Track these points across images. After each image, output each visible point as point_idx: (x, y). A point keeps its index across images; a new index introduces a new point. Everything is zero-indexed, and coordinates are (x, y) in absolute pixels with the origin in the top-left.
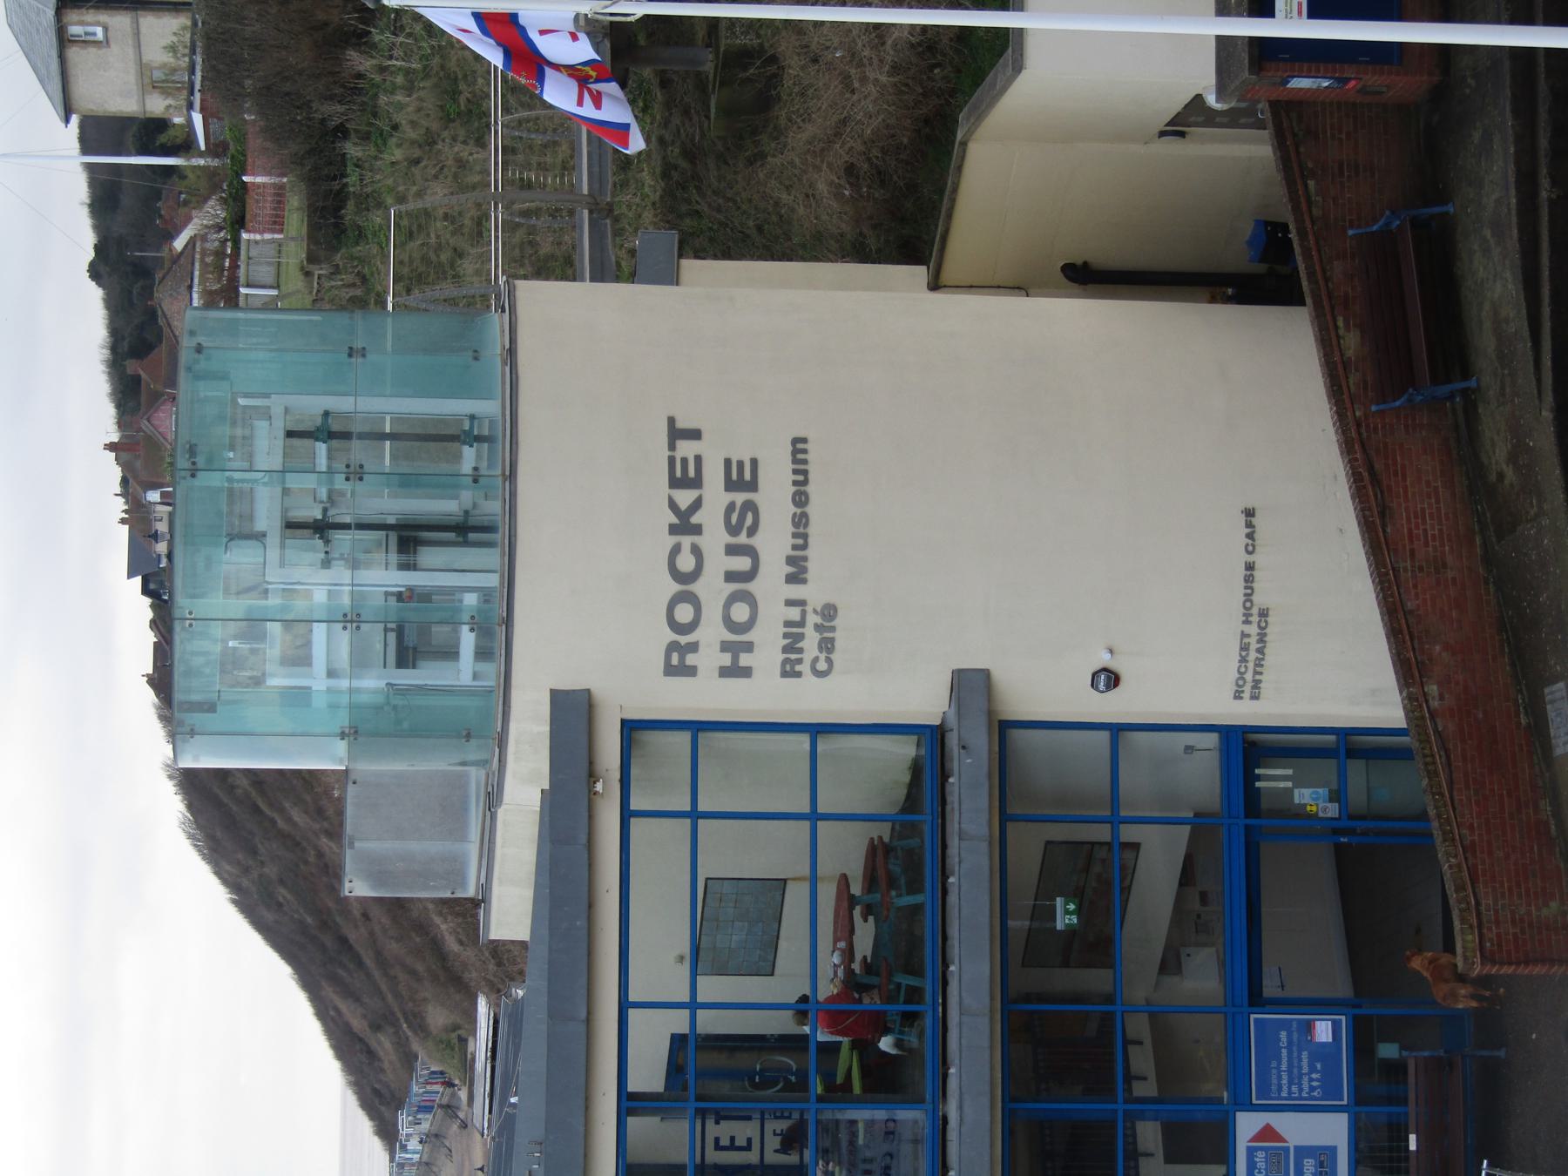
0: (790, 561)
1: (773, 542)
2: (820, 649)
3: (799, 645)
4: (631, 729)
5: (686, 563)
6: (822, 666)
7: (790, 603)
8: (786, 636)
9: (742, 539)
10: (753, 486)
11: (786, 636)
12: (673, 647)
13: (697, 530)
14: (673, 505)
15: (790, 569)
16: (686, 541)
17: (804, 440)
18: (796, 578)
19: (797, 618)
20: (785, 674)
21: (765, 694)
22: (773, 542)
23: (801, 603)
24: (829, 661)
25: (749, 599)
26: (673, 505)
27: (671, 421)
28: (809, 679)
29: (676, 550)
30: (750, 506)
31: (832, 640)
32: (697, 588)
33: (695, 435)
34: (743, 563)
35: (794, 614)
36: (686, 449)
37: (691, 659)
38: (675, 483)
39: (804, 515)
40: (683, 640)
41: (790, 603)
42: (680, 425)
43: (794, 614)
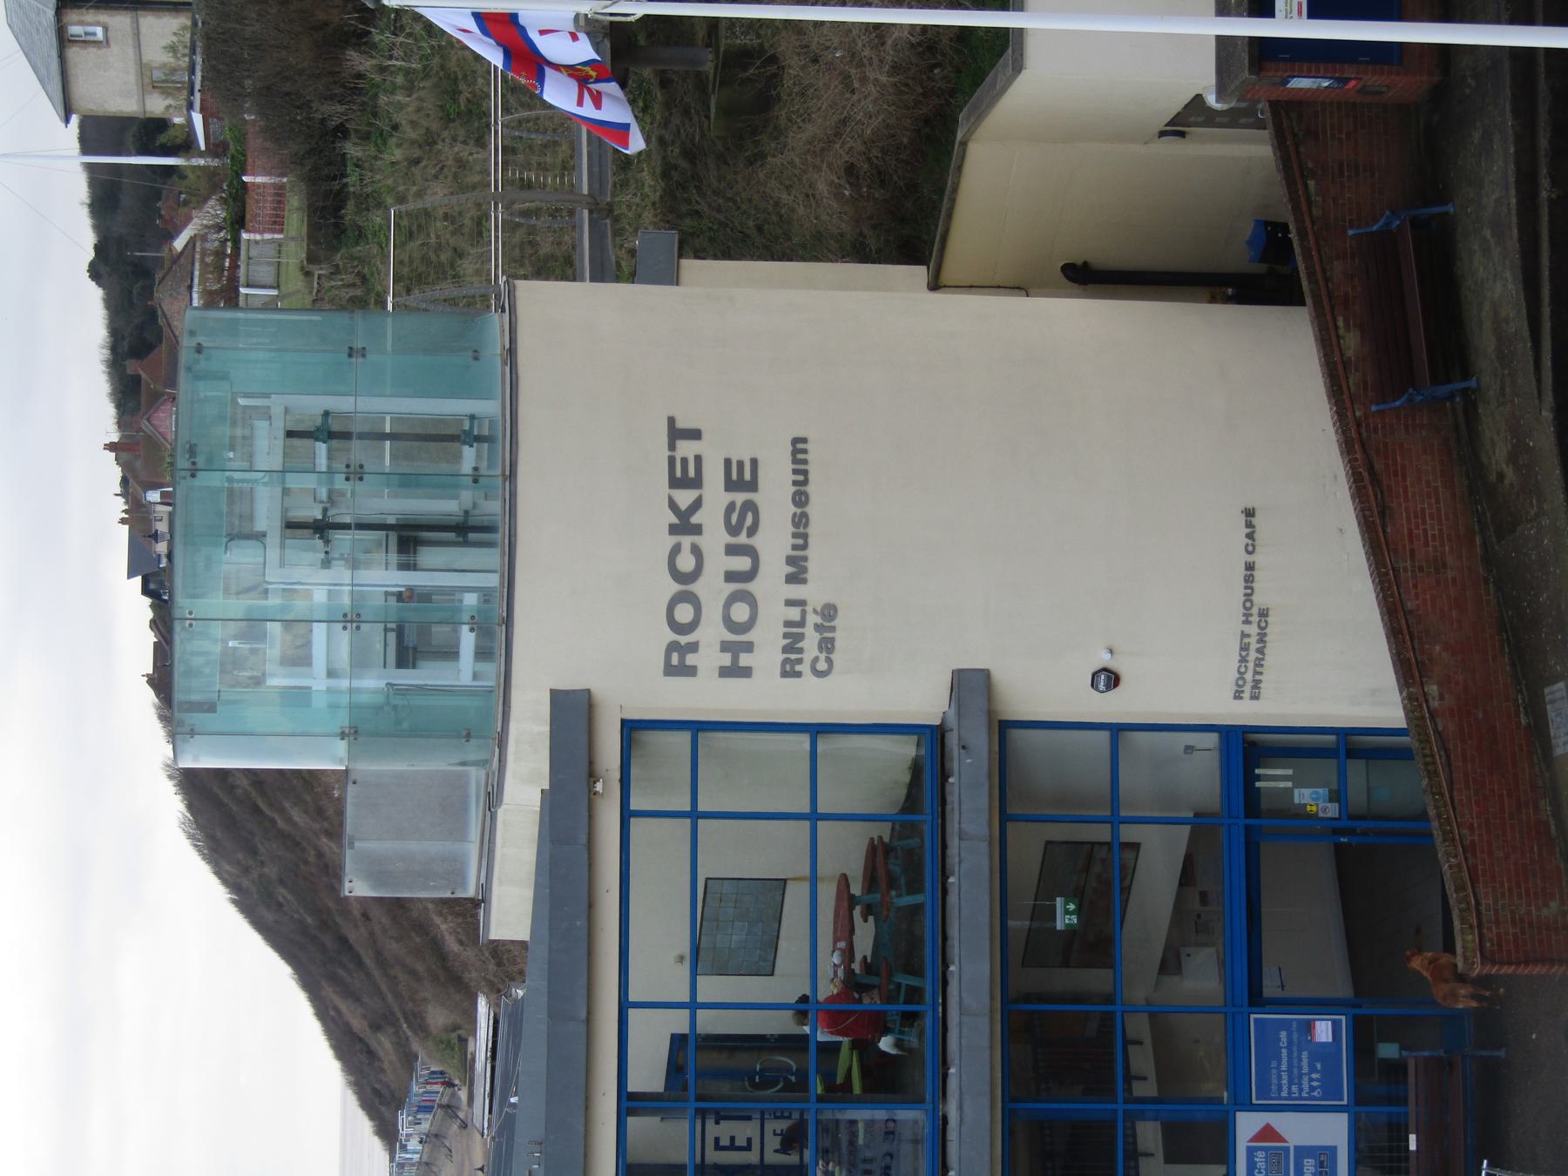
0: (790, 561)
1: (773, 542)
2: (820, 649)
3: (799, 645)
4: (631, 729)
5: (686, 563)
6: (822, 666)
7: (790, 603)
8: (786, 636)
9: (742, 539)
10: (753, 486)
11: (786, 636)
12: (673, 647)
13: (697, 530)
14: (673, 505)
15: (790, 569)
16: (686, 541)
17: (804, 440)
18: (796, 578)
19: (797, 618)
20: (785, 674)
21: (765, 694)
22: (773, 542)
23: (801, 603)
24: (829, 661)
25: (749, 599)
26: (673, 505)
27: (671, 421)
28: (809, 679)
29: (676, 550)
30: (750, 506)
31: (832, 640)
32: (697, 588)
33: (695, 435)
34: (743, 563)
35: (794, 614)
36: (686, 449)
37: (691, 659)
38: (675, 483)
39: (804, 515)
40: (683, 640)
41: (790, 603)
42: (680, 425)
43: (794, 614)
